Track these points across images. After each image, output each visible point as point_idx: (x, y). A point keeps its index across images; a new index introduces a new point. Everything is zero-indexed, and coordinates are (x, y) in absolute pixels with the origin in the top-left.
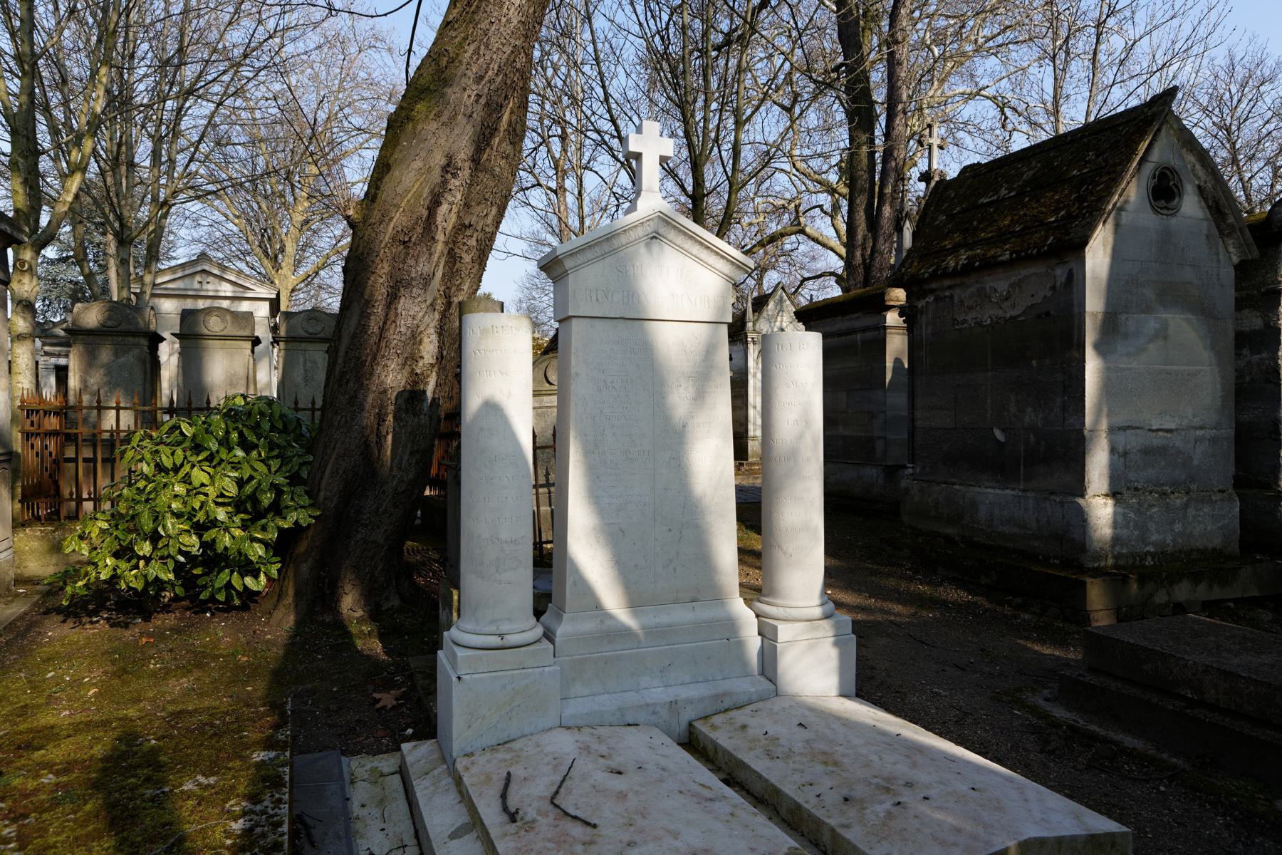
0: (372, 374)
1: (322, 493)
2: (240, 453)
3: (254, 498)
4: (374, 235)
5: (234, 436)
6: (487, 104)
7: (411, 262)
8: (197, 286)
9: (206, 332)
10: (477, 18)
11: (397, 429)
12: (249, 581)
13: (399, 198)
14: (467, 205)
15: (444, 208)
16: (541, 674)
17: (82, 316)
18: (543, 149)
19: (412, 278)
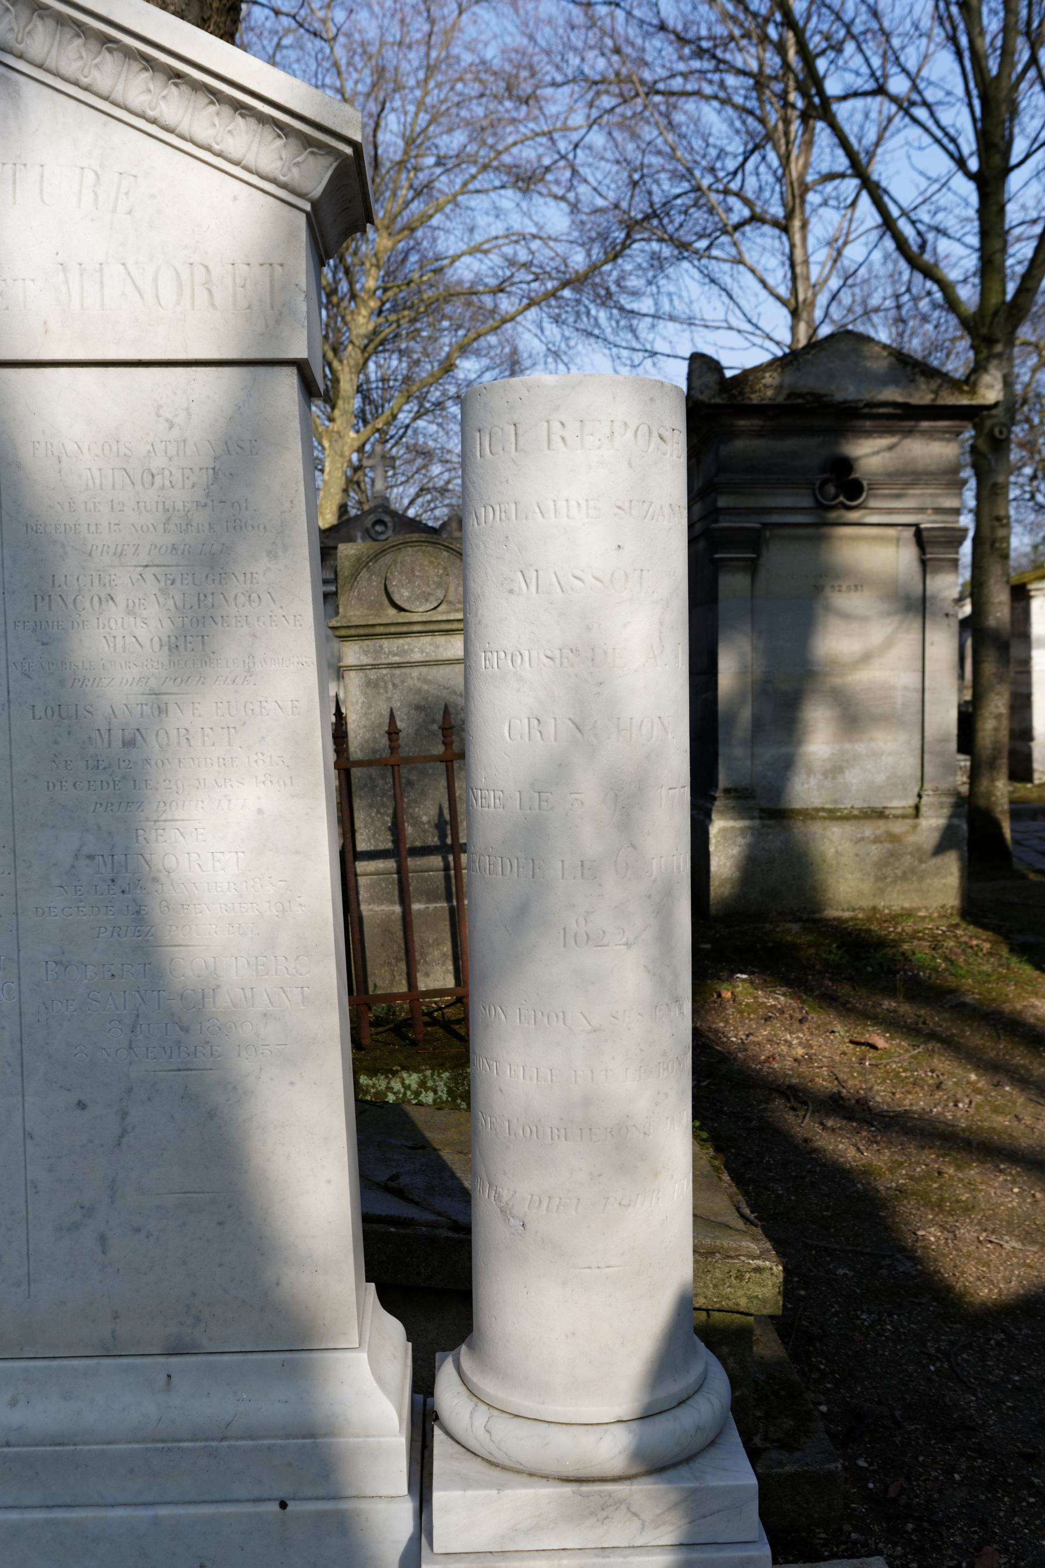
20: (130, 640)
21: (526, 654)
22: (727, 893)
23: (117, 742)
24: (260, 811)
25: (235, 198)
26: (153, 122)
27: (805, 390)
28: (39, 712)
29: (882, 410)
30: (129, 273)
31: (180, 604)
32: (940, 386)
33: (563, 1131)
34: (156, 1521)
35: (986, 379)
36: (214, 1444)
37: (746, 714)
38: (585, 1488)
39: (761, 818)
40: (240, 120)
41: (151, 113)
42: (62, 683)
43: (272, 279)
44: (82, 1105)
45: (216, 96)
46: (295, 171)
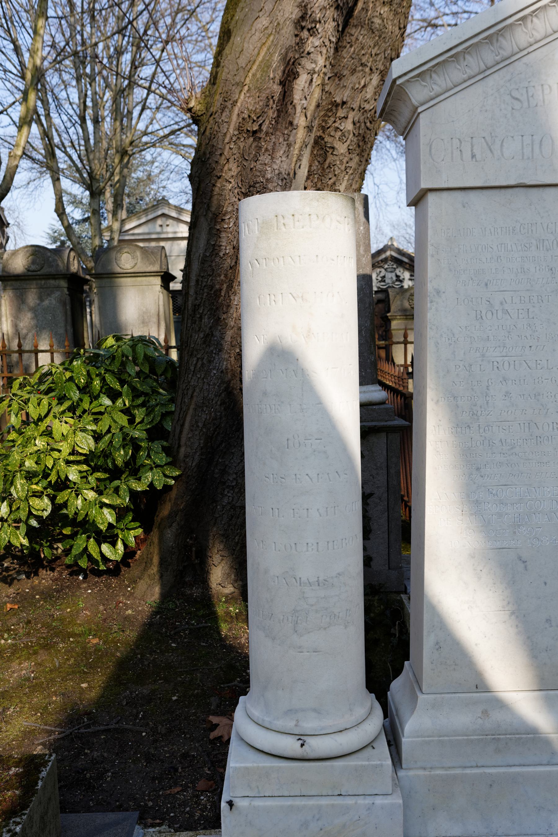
0: (229, 306)
1: (182, 450)
2: (107, 402)
3: (106, 454)
4: (216, 128)
5: (97, 383)
7: (265, 158)
8: (158, 229)
9: (118, 270)
12: (106, 548)
13: (241, 72)
14: (337, 76)
15: (301, 82)
16: (370, 808)
17: (10, 262)
19: (267, 180)
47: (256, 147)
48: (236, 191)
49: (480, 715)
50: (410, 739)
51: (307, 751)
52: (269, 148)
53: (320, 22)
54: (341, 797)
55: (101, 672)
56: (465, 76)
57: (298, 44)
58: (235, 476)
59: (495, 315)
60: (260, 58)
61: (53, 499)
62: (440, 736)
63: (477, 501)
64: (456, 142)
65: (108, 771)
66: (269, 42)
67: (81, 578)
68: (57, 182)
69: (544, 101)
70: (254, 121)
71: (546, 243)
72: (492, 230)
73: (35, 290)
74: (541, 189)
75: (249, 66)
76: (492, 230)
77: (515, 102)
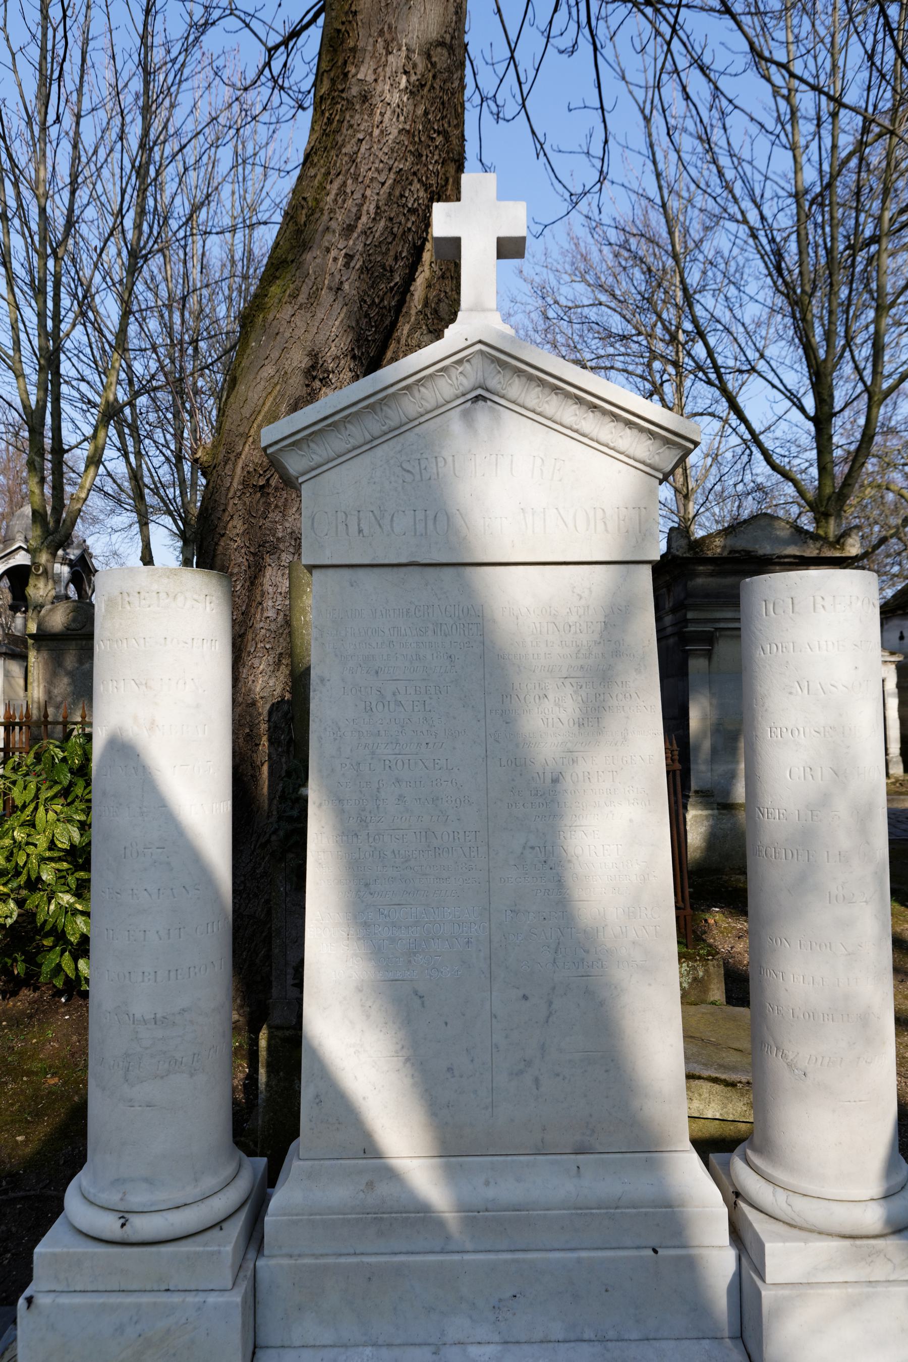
6: (364, 269)
7: (275, 516)
10: (340, 139)
11: (275, 757)
17: (47, 619)
18: (727, 426)
19: (278, 539)
20: (556, 720)
21: (801, 730)
22: (698, 856)
23: (548, 780)
24: (631, 821)
25: (619, 472)
26: (576, 431)
27: (740, 548)
28: (504, 763)
29: (786, 560)
30: (559, 513)
31: (585, 699)
32: (822, 545)
33: (831, 1016)
34: (579, 1261)
35: (850, 541)
36: (612, 1211)
37: (707, 745)
38: (858, 1242)
39: (718, 809)
40: (628, 430)
41: (575, 427)
42: (517, 745)
43: (640, 516)
44: (525, 997)
45: (615, 416)
46: (657, 457)
47: (264, 503)
48: (243, 551)
49: (362, 1188)
50: (274, 1218)
51: (129, 1233)
52: (280, 504)
53: (333, 372)
54: (169, 1293)
55: (47, 1121)
56: (349, 446)
57: (310, 394)
58: (242, 878)
59: (386, 707)
60: (266, 408)
61: (20, 903)
62: (311, 1215)
63: (365, 923)
64: (341, 516)
65: (9, 1251)
66: (275, 392)
67: (63, 1000)
68: (144, 527)
69: (438, 474)
70: (261, 475)
71: (444, 627)
72: (384, 612)
73: (74, 652)
74: (438, 568)
75: (253, 417)
76: (384, 612)
77: (407, 475)
